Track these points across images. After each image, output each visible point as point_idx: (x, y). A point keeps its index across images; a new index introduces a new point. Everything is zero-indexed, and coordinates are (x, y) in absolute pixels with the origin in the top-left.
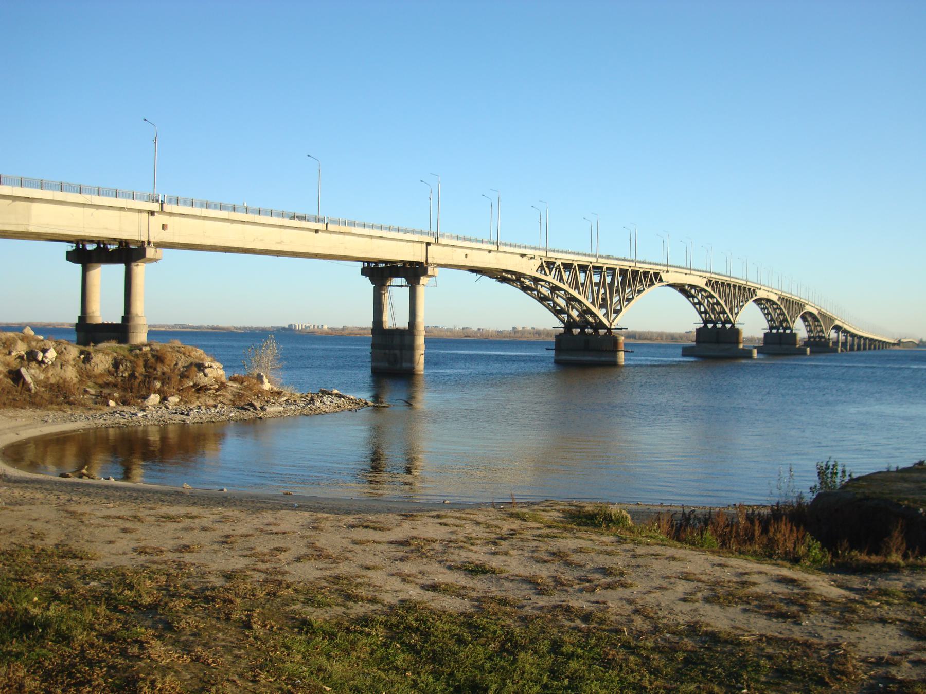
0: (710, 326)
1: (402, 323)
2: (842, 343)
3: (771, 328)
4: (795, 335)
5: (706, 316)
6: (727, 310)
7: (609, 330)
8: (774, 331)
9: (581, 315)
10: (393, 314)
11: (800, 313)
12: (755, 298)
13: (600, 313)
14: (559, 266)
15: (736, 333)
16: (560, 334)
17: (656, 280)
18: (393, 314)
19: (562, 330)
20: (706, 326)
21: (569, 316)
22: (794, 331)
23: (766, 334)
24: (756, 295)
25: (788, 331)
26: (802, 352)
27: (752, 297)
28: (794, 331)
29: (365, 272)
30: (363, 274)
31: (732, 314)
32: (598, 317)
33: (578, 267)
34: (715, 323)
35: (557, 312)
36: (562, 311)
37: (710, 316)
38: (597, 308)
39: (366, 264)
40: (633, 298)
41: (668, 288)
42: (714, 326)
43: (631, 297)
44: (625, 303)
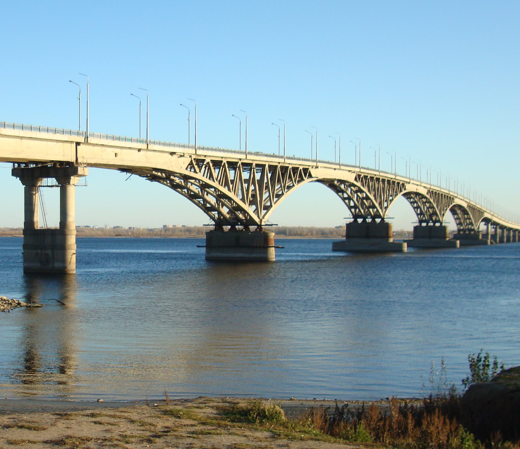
0: (360, 221)
1: (54, 223)
2: (491, 235)
3: (421, 221)
4: (444, 228)
5: (355, 211)
6: (377, 205)
7: (260, 226)
8: (424, 224)
9: (230, 212)
10: (44, 214)
11: (449, 206)
12: (404, 192)
13: (250, 210)
14: (208, 163)
15: (385, 227)
16: (211, 231)
17: (305, 176)
18: (44, 214)
19: (213, 228)
20: (355, 221)
21: (220, 213)
22: (443, 224)
23: (416, 228)
24: (405, 189)
25: (438, 224)
26: (451, 245)
27: (401, 191)
28: (443, 224)
29: (15, 173)
30: (12, 175)
31: (381, 208)
32: (248, 214)
33: (228, 164)
34: (365, 218)
35: (208, 209)
36: (213, 209)
37: (359, 210)
38: (247, 204)
39: (16, 165)
40: (283, 194)
41: (317, 183)
42: (364, 221)
43: (280, 193)
44: (275, 199)
